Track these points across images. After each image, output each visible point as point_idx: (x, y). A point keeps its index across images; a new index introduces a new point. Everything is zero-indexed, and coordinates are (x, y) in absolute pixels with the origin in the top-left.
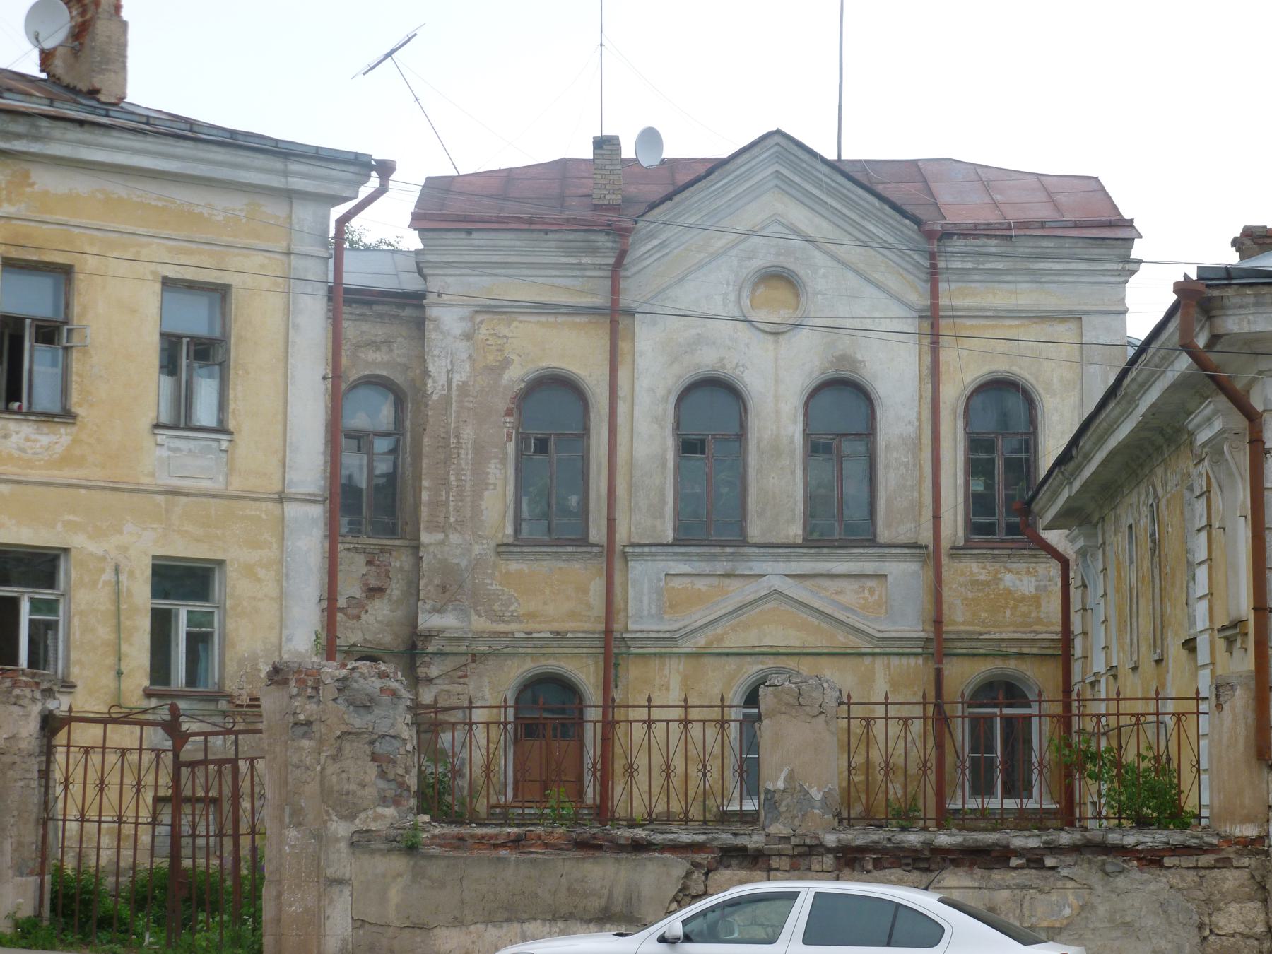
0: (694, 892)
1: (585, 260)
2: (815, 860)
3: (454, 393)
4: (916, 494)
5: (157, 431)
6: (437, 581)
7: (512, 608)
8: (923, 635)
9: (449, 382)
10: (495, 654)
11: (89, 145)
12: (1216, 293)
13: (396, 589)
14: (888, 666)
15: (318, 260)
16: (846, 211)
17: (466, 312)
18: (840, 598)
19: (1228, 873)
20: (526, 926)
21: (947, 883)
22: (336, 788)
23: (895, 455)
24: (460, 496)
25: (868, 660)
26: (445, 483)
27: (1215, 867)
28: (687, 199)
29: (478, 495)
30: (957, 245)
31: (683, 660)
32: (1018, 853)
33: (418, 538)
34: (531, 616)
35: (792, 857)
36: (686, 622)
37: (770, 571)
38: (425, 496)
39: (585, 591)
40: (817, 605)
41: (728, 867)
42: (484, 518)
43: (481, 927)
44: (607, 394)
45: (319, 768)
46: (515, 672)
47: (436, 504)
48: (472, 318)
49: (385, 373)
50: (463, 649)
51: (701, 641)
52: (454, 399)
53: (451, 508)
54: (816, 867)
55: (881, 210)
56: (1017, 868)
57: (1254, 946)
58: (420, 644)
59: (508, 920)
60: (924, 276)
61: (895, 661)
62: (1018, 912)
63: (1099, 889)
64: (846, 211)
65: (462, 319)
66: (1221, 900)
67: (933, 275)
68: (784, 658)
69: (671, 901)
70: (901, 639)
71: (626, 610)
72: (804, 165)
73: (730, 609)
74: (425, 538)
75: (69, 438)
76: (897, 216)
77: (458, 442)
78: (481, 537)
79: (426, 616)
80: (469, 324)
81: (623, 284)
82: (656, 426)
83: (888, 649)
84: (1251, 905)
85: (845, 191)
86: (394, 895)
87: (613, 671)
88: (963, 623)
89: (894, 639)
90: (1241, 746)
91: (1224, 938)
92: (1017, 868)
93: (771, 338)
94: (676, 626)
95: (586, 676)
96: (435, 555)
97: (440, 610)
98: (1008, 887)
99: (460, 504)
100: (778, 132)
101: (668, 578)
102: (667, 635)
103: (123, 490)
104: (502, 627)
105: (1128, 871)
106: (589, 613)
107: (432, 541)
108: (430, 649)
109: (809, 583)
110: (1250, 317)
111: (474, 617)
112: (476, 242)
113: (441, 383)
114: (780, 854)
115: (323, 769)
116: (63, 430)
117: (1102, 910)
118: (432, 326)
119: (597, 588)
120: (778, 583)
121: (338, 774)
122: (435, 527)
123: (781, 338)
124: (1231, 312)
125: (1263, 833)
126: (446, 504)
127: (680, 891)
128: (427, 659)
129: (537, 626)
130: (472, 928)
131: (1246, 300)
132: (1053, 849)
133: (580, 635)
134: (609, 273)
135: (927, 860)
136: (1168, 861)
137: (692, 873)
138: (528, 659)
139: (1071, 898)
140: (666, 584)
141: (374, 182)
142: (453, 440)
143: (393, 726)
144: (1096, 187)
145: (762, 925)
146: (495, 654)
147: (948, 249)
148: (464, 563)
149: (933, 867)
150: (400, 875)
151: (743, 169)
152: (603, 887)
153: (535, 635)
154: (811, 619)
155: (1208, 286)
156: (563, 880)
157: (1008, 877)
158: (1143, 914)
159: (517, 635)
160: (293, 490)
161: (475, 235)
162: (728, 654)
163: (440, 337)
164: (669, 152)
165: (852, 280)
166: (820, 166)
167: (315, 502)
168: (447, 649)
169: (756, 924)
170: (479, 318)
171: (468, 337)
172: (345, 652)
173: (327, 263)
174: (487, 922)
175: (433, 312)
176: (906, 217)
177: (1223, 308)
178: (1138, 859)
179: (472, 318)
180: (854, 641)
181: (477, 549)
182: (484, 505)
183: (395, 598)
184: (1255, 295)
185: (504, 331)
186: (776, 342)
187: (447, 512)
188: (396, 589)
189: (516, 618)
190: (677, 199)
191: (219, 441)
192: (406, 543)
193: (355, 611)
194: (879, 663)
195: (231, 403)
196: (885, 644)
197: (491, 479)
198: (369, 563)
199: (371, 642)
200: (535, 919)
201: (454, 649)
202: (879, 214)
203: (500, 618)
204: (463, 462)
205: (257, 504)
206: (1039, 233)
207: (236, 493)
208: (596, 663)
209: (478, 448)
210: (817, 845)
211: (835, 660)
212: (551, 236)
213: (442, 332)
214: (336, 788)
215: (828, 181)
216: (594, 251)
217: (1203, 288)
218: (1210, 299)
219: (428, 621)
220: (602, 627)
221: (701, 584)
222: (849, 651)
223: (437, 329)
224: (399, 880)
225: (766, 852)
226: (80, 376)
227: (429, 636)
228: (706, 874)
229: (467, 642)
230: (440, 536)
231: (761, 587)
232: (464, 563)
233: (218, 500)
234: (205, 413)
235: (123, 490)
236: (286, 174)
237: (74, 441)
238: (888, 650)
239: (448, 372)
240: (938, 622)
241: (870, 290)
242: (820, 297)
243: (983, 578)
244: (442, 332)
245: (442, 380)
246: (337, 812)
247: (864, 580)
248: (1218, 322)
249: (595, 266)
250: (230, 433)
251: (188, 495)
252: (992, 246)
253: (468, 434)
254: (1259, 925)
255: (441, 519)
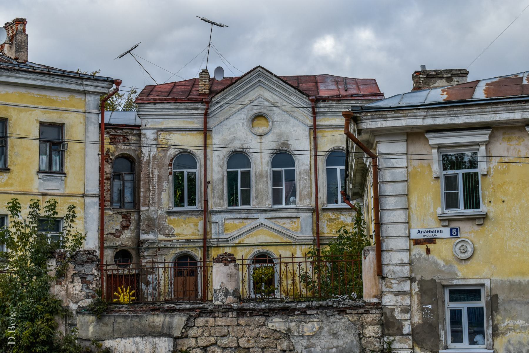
0: (190, 325)
1: (195, 112)
2: (230, 313)
3: (151, 159)
4: (310, 189)
5: (38, 174)
6: (146, 223)
7: (172, 232)
8: (313, 238)
9: (149, 155)
10: (166, 248)
11: (12, 77)
12: (358, 115)
13: (132, 227)
14: (301, 249)
15: (95, 115)
16: (284, 93)
17: (155, 131)
18: (285, 226)
19: (369, 316)
20: (135, 338)
21: (274, 320)
22: (72, 293)
23: (302, 176)
24: (154, 194)
25: (294, 247)
26: (149, 190)
27: (364, 314)
28: (229, 90)
29: (160, 194)
30: (321, 104)
31: (231, 248)
32: (298, 310)
33: (139, 209)
34: (179, 235)
35: (222, 312)
36: (231, 235)
37: (260, 217)
38: (142, 194)
39: (197, 226)
40: (276, 228)
41: (202, 316)
42: (162, 201)
43: (119, 339)
44: (203, 158)
45: (66, 286)
46: (174, 252)
47: (146, 197)
48: (157, 133)
49: (128, 153)
50: (155, 246)
51: (237, 241)
52: (151, 161)
53: (151, 198)
54: (231, 316)
55: (296, 92)
56: (298, 315)
57: (378, 341)
58: (141, 245)
59: (129, 337)
60: (311, 115)
61: (303, 247)
62: (298, 330)
63: (325, 322)
64: (284, 93)
65: (153, 133)
66: (366, 325)
67: (314, 113)
68: (265, 246)
69: (183, 329)
70: (305, 239)
71: (211, 231)
72: (269, 78)
73: (246, 230)
74: (142, 209)
75: (7, 177)
76: (301, 94)
77: (153, 176)
78: (161, 208)
79: (143, 235)
80: (156, 135)
81: (208, 120)
82: (220, 168)
83: (301, 242)
84: (377, 326)
85: (283, 86)
86: (91, 329)
87: (207, 253)
88: (327, 233)
89: (303, 239)
90: (372, 271)
91: (367, 338)
92: (298, 315)
93: (259, 137)
94: (228, 237)
95: (198, 254)
96: (145, 214)
97: (148, 233)
98: (294, 321)
99: (154, 196)
100: (259, 67)
101: (225, 220)
102: (225, 240)
103: (27, 194)
104: (169, 238)
105: (335, 315)
106: (198, 233)
107: (145, 210)
108: (144, 246)
109: (273, 221)
110: (370, 123)
111: (159, 236)
112: (157, 107)
113: (146, 156)
114: (218, 311)
115: (67, 286)
116: (5, 174)
117: (326, 329)
118: (143, 136)
119: (201, 224)
120: (262, 221)
121: (72, 288)
122: (145, 205)
123: (262, 137)
124: (363, 121)
125: (380, 301)
126: (149, 197)
127: (186, 325)
128: (143, 250)
129: (181, 238)
130: (117, 340)
131: (368, 117)
132: (309, 308)
133: (195, 240)
134: (203, 117)
135: (268, 313)
136: (348, 311)
137: (190, 318)
138: (178, 249)
139: (316, 325)
140: (224, 222)
141: (114, 87)
142: (151, 175)
143: (91, 271)
144: (374, 82)
145: (213, 336)
146: (166, 248)
147: (319, 105)
148: (155, 217)
149: (270, 315)
150: (93, 322)
151: (248, 80)
152: (160, 325)
153: (180, 241)
154: (274, 233)
155: (354, 113)
156: (147, 322)
157: (294, 318)
158: (340, 330)
159: (174, 241)
160: (88, 193)
161: (157, 105)
162: (246, 246)
163: (146, 140)
164: (226, 75)
165: (287, 117)
166: (274, 78)
167: (96, 197)
168: (150, 246)
169: (211, 336)
170: (159, 133)
171: (155, 139)
172: (115, 248)
173: (99, 116)
174: (122, 337)
175: (143, 131)
176: (304, 94)
177: (361, 120)
178: (338, 311)
179: (157, 133)
180: (289, 240)
181: (160, 212)
182: (162, 197)
183: (132, 229)
184: (371, 115)
185: (168, 137)
186: (261, 139)
187: (149, 199)
188: (132, 227)
189: (173, 235)
190: (225, 90)
191: (61, 177)
192: (136, 210)
193: (119, 234)
194: (298, 248)
195: (65, 164)
196: (300, 241)
197: (164, 188)
198: (123, 218)
199: (124, 244)
200: (138, 336)
201: (152, 246)
202: (295, 94)
203: (168, 236)
204: (154, 182)
205: (75, 198)
206: (350, 98)
207: (67, 195)
208: (201, 251)
209: (160, 177)
210: (230, 308)
211: (283, 247)
212: (183, 104)
213: (147, 139)
214: (72, 293)
215: (277, 83)
216: (197, 109)
217: (352, 114)
218: (357, 117)
219: (143, 237)
220: (202, 237)
221: (236, 222)
222: (287, 244)
223: (145, 137)
224: (93, 324)
225: (214, 311)
226: (11, 156)
227: (144, 242)
228: (195, 319)
229: (157, 244)
230: (147, 208)
231: (257, 222)
232: (155, 217)
233: (61, 197)
234: (56, 167)
235: (27, 194)
236: (83, 85)
237: (9, 178)
238: (301, 243)
239: (149, 152)
240: (318, 233)
241: (293, 120)
242: (275, 123)
243: (333, 217)
244: (147, 139)
245: (147, 154)
246: (72, 301)
247: (292, 219)
248: (360, 125)
249: (198, 114)
250: (65, 174)
251: (50, 195)
252: (334, 104)
253: (156, 172)
254: (379, 333)
255: (147, 202)
